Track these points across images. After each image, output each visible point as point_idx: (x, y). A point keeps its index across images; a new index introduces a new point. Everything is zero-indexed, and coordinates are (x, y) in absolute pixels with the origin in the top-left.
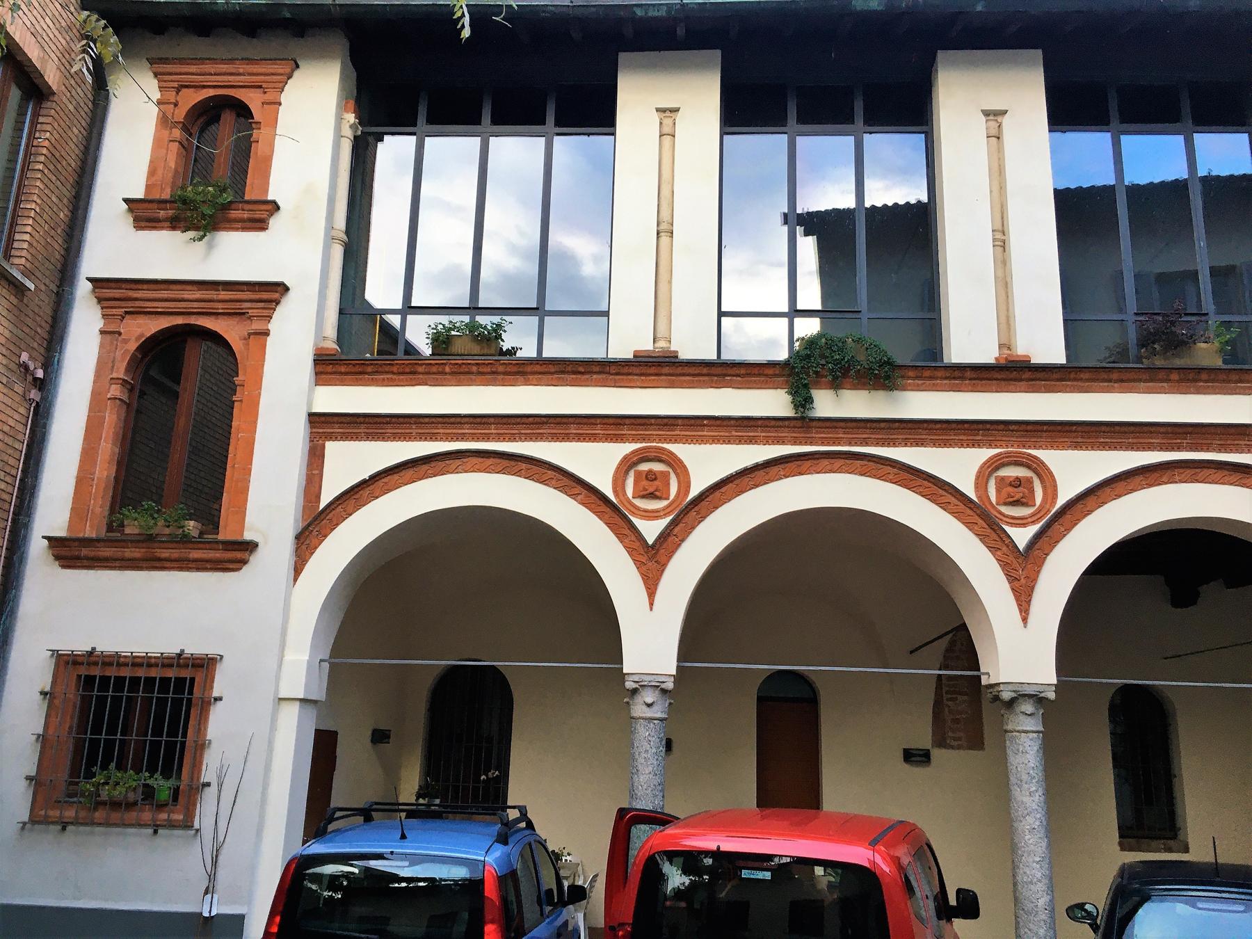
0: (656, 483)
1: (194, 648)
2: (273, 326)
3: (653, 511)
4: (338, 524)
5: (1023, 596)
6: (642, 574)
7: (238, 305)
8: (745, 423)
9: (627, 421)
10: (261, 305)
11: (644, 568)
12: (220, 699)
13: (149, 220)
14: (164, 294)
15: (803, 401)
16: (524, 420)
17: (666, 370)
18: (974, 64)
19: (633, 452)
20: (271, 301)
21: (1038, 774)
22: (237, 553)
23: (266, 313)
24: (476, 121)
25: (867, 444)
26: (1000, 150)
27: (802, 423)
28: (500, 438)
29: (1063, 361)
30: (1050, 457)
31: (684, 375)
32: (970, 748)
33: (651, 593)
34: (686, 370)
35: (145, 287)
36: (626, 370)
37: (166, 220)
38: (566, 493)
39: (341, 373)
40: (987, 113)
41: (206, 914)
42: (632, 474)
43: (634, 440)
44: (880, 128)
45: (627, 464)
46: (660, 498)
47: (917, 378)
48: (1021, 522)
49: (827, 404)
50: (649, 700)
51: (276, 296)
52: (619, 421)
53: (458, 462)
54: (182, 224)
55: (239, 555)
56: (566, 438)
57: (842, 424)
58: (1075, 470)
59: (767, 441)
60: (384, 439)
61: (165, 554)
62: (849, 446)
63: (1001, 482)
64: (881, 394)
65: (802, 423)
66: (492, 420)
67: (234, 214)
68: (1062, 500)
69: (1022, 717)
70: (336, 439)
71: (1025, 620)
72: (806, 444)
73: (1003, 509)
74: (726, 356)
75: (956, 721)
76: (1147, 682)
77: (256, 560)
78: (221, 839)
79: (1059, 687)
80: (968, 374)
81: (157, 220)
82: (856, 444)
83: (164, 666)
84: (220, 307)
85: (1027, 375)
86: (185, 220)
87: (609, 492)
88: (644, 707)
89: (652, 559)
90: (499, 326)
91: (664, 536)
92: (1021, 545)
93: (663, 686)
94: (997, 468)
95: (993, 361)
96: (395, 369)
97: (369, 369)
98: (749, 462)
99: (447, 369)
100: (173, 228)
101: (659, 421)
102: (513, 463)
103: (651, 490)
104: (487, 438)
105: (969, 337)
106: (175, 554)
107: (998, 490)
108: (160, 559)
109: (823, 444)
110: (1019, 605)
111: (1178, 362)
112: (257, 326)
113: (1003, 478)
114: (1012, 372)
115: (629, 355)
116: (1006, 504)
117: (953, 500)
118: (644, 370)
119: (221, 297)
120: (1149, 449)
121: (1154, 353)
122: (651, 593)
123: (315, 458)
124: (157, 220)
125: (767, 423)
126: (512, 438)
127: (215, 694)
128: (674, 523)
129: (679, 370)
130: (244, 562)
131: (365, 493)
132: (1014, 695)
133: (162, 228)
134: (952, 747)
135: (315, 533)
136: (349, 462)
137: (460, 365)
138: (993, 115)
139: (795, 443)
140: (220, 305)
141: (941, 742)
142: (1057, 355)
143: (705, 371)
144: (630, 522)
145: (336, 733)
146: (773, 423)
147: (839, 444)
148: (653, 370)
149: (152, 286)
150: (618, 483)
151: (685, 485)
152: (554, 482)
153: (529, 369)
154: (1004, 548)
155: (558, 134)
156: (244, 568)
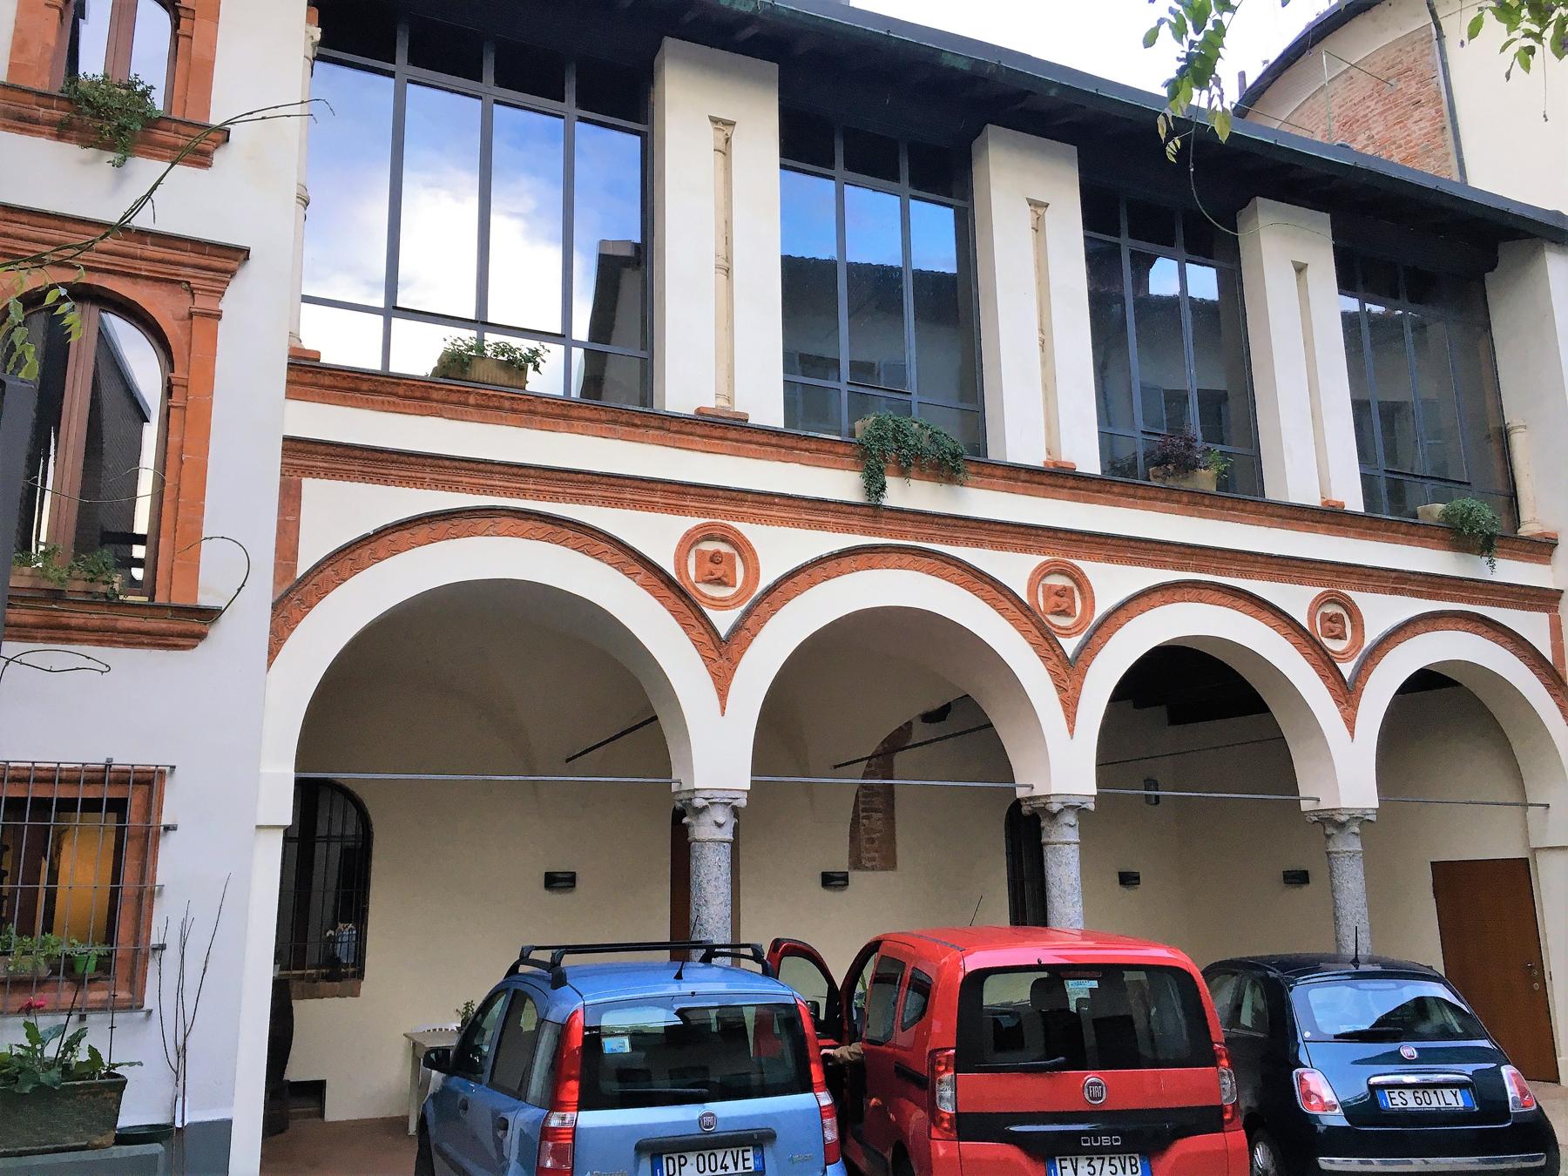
0: (722, 566)
1: (127, 755)
2: (226, 305)
3: (721, 600)
4: (327, 592)
5: (1070, 706)
6: (712, 673)
7: (129, 262)
8: (818, 505)
9: (692, 490)
10: (210, 274)
11: (715, 666)
12: (174, 828)
13: (21, 118)
14: (56, 235)
15: (875, 486)
16: (572, 476)
17: (732, 434)
18: (723, 71)
19: (697, 528)
20: (226, 271)
21: (1077, 884)
22: (189, 624)
23: (217, 286)
24: (830, 163)
25: (932, 541)
26: (728, 168)
27: (872, 511)
28: (539, 495)
29: (1099, 472)
30: (1093, 569)
31: (750, 442)
32: (883, 869)
33: (723, 694)
34: (757, 437)
35: (24, 219)
36: (688, 429)
37: (50, 123)
38: (623, 571)
39: (322, 386)
40: (1031, 202)
41: (178, 1125)
42: (693, 553)
43: (699, 513)
44: (1202, 259)
45: (690, 541)
46: (725, 584)
47: (978, 474)
48: (722, 604)
49: (901, 493)
50: (721, 820)
51: (232, 265)
52: (682, 489)
53: (488, 522)
54: (74, 134)
55: (195, 626)
56: (618, 503)
57: (911, 517)
58: (1112, 582)
59: (838, 528)
60: (386, 483)
61: (77, 620)
62: (923, 541)
63: (1048, 589)
64: (944, 489)
65: (872, 511)
66: (532, 472)
67: (160, 135)
68: (1099, 613)
69: (1065, 829)
70: (318, 476)
71: (1071, 731)
72: (875, 535)
73: (701, 587)
74: (395, 368)
75: (872, 841)
76: (330, 775)
77: (219, 633)
78: (188, 1022)
79: (1098, 798)
80: (1023, 476)
81: (36, 122)
82: (922, 540)
83: (38, 781)
84: (144, 268)
85: (1071, 483)
86: (82, 129)
87: (671, 570)
88: (714, 829)
89: (722, 654)
90: (536, 352)
91: (737, 628)
92: (723, 631)
93: (735, 803)
94: (698, 542)
95: (1041, 465)
96: (401, 391)
97: (365, 387)
98: (824, 551)
99: (472, 400)
100: (60, 137)
101: (728, 494)
102: (558, 529)
103: (718, 574)
104: (521, 493)
105: (1018, 437)
106: (95, 620)
107: (1046, 599)
108: (67, 627)
109: (891, 537)
110: (1067, 717)
111: (1186, 485)
112: (202, 303)
113: (1050, 587)
114: (1329, 518)
115: (691, 412)
116: (1053, 613)
117: (1009, 605)
118: (706, 431)
119: (147, 254)
120: (1165, 567)
121: (1167, 474)
122: (723, 694)
123: (290, 498)
124: (36, 122)
125: (839, 507)
126: (554, 497)
127: (165, 821)
128: (747, 613)
129: (747, 436)
130: (201, 636)
131: (365, 552)
132: (705, 803)
133: (40, 134)
134: (867, 869)
135: (295, 602)
136: (339, 511)
137: (489, 397)
138: (1036, 205)
139: (864, 533)
140: (143, 265)
141: (857, 864)
142: (776, 419)
143: (774, 440)
144: (703, 615)
145: (1436, 866)
146: (845, 508)
147: (906, 538)
148: (718, 433)
149: (35, 220)
150: (680, 561)
151: (753, 572)
152: (608, 557)
153: (575, 413)
154: (1055, 659)
155: (582, 119)
156: (201, 645)
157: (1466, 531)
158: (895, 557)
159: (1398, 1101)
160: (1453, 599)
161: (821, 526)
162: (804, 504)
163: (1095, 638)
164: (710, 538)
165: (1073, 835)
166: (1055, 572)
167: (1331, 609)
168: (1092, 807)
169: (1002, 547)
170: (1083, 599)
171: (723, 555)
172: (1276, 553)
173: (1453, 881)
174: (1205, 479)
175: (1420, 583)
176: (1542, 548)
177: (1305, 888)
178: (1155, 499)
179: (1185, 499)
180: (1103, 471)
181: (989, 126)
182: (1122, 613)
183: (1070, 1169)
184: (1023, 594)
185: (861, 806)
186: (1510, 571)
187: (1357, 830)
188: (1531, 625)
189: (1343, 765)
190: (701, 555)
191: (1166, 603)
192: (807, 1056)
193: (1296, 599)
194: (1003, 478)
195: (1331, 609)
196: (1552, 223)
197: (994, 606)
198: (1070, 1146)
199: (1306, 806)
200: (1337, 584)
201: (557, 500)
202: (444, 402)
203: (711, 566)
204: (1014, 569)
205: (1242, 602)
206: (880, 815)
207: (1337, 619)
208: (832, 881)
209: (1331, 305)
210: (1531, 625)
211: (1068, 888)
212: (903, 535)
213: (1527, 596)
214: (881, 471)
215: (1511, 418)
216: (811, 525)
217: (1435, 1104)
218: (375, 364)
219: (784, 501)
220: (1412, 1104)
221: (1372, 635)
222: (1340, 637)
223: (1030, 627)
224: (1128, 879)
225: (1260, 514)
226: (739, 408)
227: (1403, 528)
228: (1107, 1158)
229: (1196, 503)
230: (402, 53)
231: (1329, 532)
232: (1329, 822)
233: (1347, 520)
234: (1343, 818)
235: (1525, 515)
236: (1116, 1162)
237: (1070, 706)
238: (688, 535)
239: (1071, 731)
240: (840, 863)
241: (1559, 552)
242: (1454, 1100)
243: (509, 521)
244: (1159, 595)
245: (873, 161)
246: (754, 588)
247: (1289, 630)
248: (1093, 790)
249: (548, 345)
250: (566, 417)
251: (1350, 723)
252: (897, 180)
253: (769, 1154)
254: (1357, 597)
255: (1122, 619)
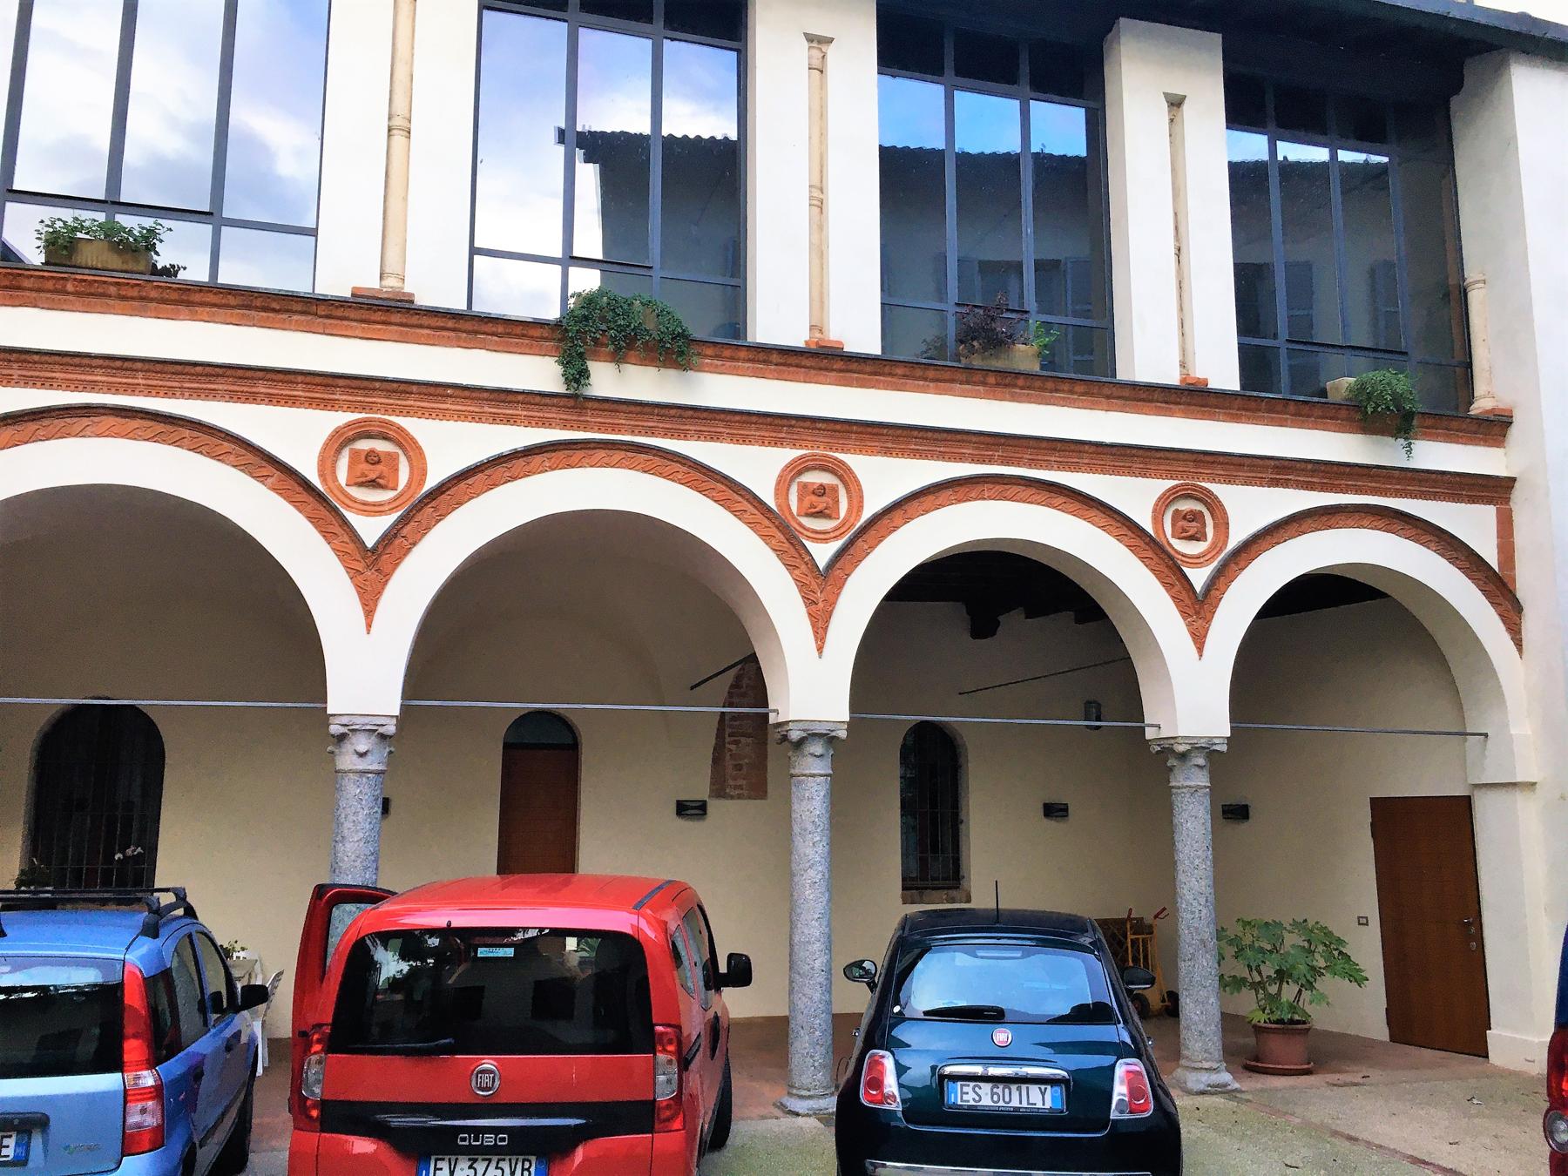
0: (379, 467)
3: (365, 504)
5: (820, 621)
6: (357, 586)
11: (360, 578)
15: (577, 376)
17: (396, 318)
21: (823, 822)
25: (653, 435)
28: (150, 391)
31: (421, 326)
34: (425, 321)
36: (339, 313)
40: (810, 38)
43: (352, 407)
45: (340, 440)
47: (717, 357)
49: (605, 380)
50: (362, 748)
59: (530, 422)
65: (575, 402)
68: (867, 514)
69: (810, 759)
71: (820, 649)
79: (852, 725)
80: (775, 357)
85: (839, 365)
88: (355, 757)
89: (372, 567)
91: (388, 538)
93: (381, 730)
94: (800, 473)
95: (802, 344)
98: (505, 448)
99: (70, 287)
103: (373, 476)
104: (131, 390)
105: (1145, 353)
107: (800, 500)
114: (1192, 398)
115: (347, 294)
120: (961, 460)
121: (972, 351)
126: (170, 393)
129: (415, 320)
132: (344, 730)
134: (732, 797)
139: (564, 427)
141: (719, 791)
143: (450, 324)
144: (345, 523)
145: (1378, 805)
147: (620, 432)
148: (378, 316)
151: (419, 472)
152: (232, 458)
154: (803, 567)
157: (1370, 410)
158: (602, 453)
159: (965, 1096)
160: (1359, 491)
161: (509, 420)
162: (486, 395)
163: (860, 542)
164: (369, 436)
165: (820, 767)
166: (814, 468)
167: (1186, 506)
168: (843, 734)
169: (745, 440)
170: (850, 498)
171: (372, 451)
172: (1108, 439)
173: (1391, 818)
174: (1024, 357)
175: (1313, 472)
176: (1495, 428)
177: (1244, 826)
178: (952, 381)
179: (992, 380)
180: (1243, 387)
181: (1122, 20)
182: (898, 514)
183: (446, 1171)
184: (769, 499)
185: (728, 731)
186: (1434, 455)
187: (1201, 761)
188: (1472, 524)
189: (1191, 689)
190: (355, 455)
191: (960, 501)
192: (122, 1027)
193: (1136, 496)
194: (749, 360)
195: (1186, 506)
196: (1515, 28)
197: (728, 508)
198: (446, 1144)
199: (1150, 734)
200: (1197, 476)
201: (174, 396)
202: (39, 290)
203: (365, 467)
204: (758, 467)
205: (1061, 499)
206: (749, 740)
207: (1196, 517)
208: (689, 810)
209: (1216, 145)
210: (1472, 524)
211: (810, 827)
212: (615, 428)
213: (1462, 486)
214: (581, 355)
215: (1471, 274)
216: (495, 419)
217: (1015, 1103)
218: (460, 305)
219: (458, 392)
220: (986, 1101)
221: (1238, 534)
222: (1198, 537)
223: (774, 531)
224: (1054, 811)
225: (1092, 395)
226: (408, 288)
227: (1292, 407)
228: (495, 1158)
229: (1009, 384)
230: (949, 63)
231: (1187, 415)
232: (1167, 756)
233: (1212, 400)
234: (1181, 748)
235: (1480, 388)
236: (505, 1165)
237: (820, 621)
238: (337, 432)
239: (820, 649)
240: (699, 789)
241: (1514, 432)
242: (1042, 1100)
243: (111, 420)
244: (950, 492)
245: (986, 64)
246: (859, 515)
247: (1124, 531)
248: (845, 716)
249: (167, 223)
250: (189, 304)
251: (1199, 639)
252: (650, 21)
253: (37, 1141)
254: (1220, 490)
255: (897, 521)
